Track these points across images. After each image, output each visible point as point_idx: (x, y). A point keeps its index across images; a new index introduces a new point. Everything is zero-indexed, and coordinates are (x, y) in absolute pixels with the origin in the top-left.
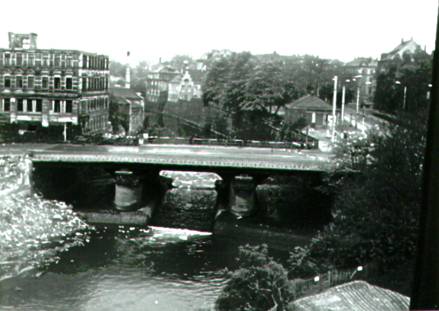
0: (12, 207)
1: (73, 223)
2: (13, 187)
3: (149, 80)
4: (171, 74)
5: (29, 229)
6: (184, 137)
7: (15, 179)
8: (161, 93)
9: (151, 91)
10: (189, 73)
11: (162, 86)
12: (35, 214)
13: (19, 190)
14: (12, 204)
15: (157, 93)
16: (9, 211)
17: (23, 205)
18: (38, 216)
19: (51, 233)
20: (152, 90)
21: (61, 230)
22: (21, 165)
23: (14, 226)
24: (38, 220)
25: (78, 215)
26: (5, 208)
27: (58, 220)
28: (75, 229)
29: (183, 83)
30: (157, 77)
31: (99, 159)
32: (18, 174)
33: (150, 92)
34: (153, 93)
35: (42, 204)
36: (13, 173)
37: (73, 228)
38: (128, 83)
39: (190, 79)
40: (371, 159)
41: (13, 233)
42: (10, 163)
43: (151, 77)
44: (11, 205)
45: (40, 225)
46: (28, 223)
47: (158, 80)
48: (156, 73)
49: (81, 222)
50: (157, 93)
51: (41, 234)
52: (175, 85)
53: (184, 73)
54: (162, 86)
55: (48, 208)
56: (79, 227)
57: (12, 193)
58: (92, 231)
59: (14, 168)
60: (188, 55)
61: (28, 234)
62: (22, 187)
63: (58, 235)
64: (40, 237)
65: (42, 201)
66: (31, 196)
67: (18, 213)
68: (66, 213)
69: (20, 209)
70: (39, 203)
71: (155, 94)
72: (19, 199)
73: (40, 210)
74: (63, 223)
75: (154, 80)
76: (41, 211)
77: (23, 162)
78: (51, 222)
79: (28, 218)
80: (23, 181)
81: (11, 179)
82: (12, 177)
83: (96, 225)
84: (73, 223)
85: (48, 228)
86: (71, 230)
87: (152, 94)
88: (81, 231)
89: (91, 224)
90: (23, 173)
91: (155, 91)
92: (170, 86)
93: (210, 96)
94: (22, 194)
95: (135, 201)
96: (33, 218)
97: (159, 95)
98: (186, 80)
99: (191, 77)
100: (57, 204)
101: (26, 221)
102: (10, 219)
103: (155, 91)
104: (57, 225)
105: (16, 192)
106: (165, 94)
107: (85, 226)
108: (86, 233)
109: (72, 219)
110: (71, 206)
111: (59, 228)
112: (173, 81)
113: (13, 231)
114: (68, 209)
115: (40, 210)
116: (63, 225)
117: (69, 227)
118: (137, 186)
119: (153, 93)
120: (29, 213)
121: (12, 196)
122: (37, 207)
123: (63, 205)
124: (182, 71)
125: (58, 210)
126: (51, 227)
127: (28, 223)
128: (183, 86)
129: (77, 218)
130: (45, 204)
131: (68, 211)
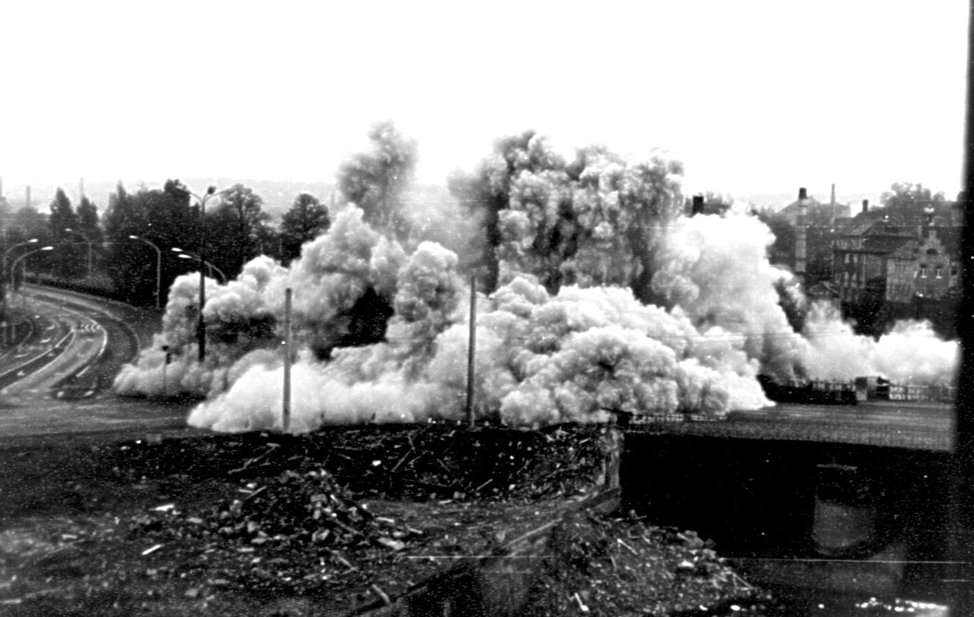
0: (587, 538)
1: (720, 583)
2: (584, 494)
3: (840, 253)
4: (893, 238)
5: (627, 589)
6: (56, 274)
7: (591, 473)
8: (869, 282)
9: (843, 275)
10: (938, 236)
11: (871, 264)
12: (635, 556)
13: (599, 500)
14: (587, 530)
15: (859, 283)
16: (583, 546)
17: (610, 533)
18: (644, 561)
19: (673, 604)
20: (847, 276)
21: (696, 596)
22: (603, 443)
23: (594, 583)
24: (643, 569)
25: (729, 564)
26: (576, 541)
27: (687, 570)
28: (726, 596)
29: (924, 259)
30: (859, 245)
31: (777, 435)
32: (598, 463)
33: (842, 281)
34: (850, 281)
35: (647, 532)
36: (586, 461)
37: (722, 593)
38: (801, 260)
39: (940, 250)
40: (703, 362)
41: (592, 599)
42: (580, 437)
43: (844, 246)
44: (586, 534)
45: (650, 583)
46: (624, 576)
47: (860, 253)
48: (857, 237)
49: (737, 581)
50: (859, 283)
51: (653, 603)
52: (902, 263)
53: (926, 235)
54: (871, 264)
55: (662, 543)
56: (735, 592)
57: (586, 504)
58: (766, 602)
59: (588, 449)
60: (723, 217)
61: (626, 601)
62: (605, 494)
63: (690, 607)
64: (652, 609)
65: (647, 527)
66: (625, 514)
67: (601, 550)
68: (703, 558)
69: (604, 543)
70: (642, 531)
71: (854, 285)
72: (602, 519)
73: (645, 546)
74: (700, 581)
75: (852, 252)
76: (649, 549)
77: (608, 435)
78: (671, 576)
79: (621, 564)
80: (607, 479)
81: (585, 475)
82: (585, 468)
83: (776, 588)
84: (720, 583)
85: (666, 590)
86: (718, 597)
87: (846, 284)
88: (740, 601)
89: (764, 586)
90: (608, 460)
91: (854, 277)
92: (891, 266)
93: (416, 283)
94: (604, 507)
95: (503, 422)
96: (633, 564)
97: (863, 287)
98: (932, 252)
99: (943, 243)
100: (680, 535)
101: (618, 572)
102: (587, 565)
103: (854, 277)
104: (687, 585)
105: (591, 503)
106: (880, 283)
107: (747, 589)
108: (754, 607)
109: (717, 572)
110: (709, 542)
111: (691, 591)
112: (898, 254)
113: (594, 593)
114: (705, 547)
115: (645, 546)
116: (699, 586)
117: (713, 591)
118: (867, 501)
119: (850, 281)
120: (623, 553)
121: (587, 513)
122: (638, 541)
123: (691, 538)
124: (920, 229)
125: (684, 550)
126: (674, 586)
127: (624, 576)
128: (923, 266)
129: (728, 571)
130: (654, 534)
131: (706, 551)
